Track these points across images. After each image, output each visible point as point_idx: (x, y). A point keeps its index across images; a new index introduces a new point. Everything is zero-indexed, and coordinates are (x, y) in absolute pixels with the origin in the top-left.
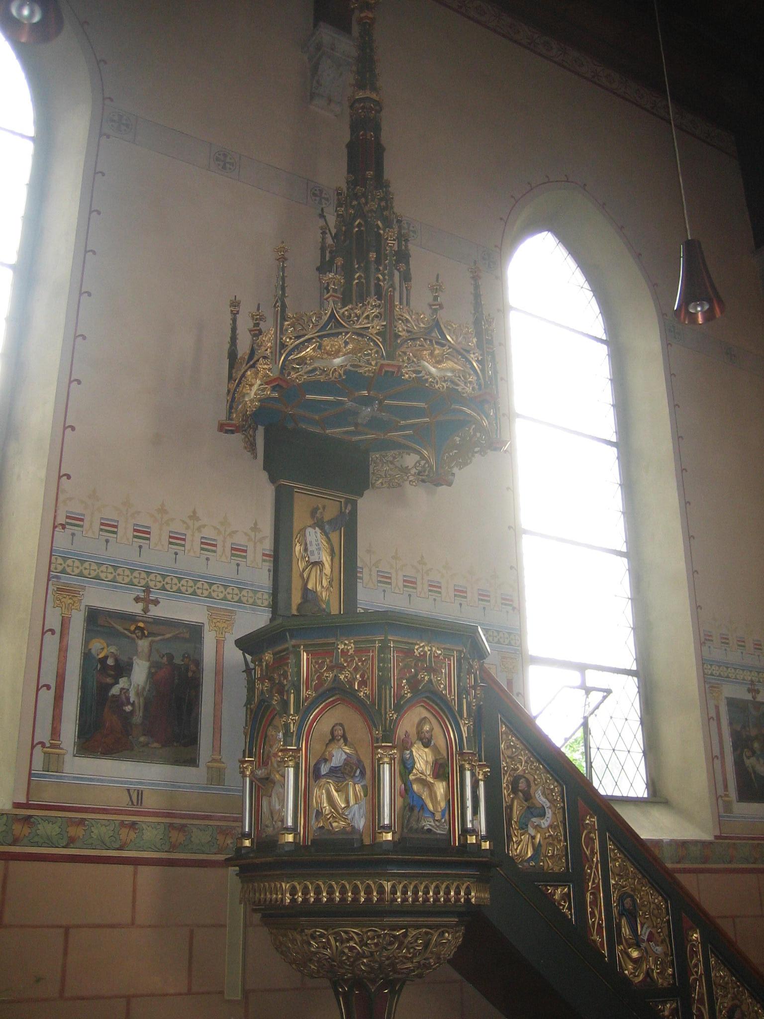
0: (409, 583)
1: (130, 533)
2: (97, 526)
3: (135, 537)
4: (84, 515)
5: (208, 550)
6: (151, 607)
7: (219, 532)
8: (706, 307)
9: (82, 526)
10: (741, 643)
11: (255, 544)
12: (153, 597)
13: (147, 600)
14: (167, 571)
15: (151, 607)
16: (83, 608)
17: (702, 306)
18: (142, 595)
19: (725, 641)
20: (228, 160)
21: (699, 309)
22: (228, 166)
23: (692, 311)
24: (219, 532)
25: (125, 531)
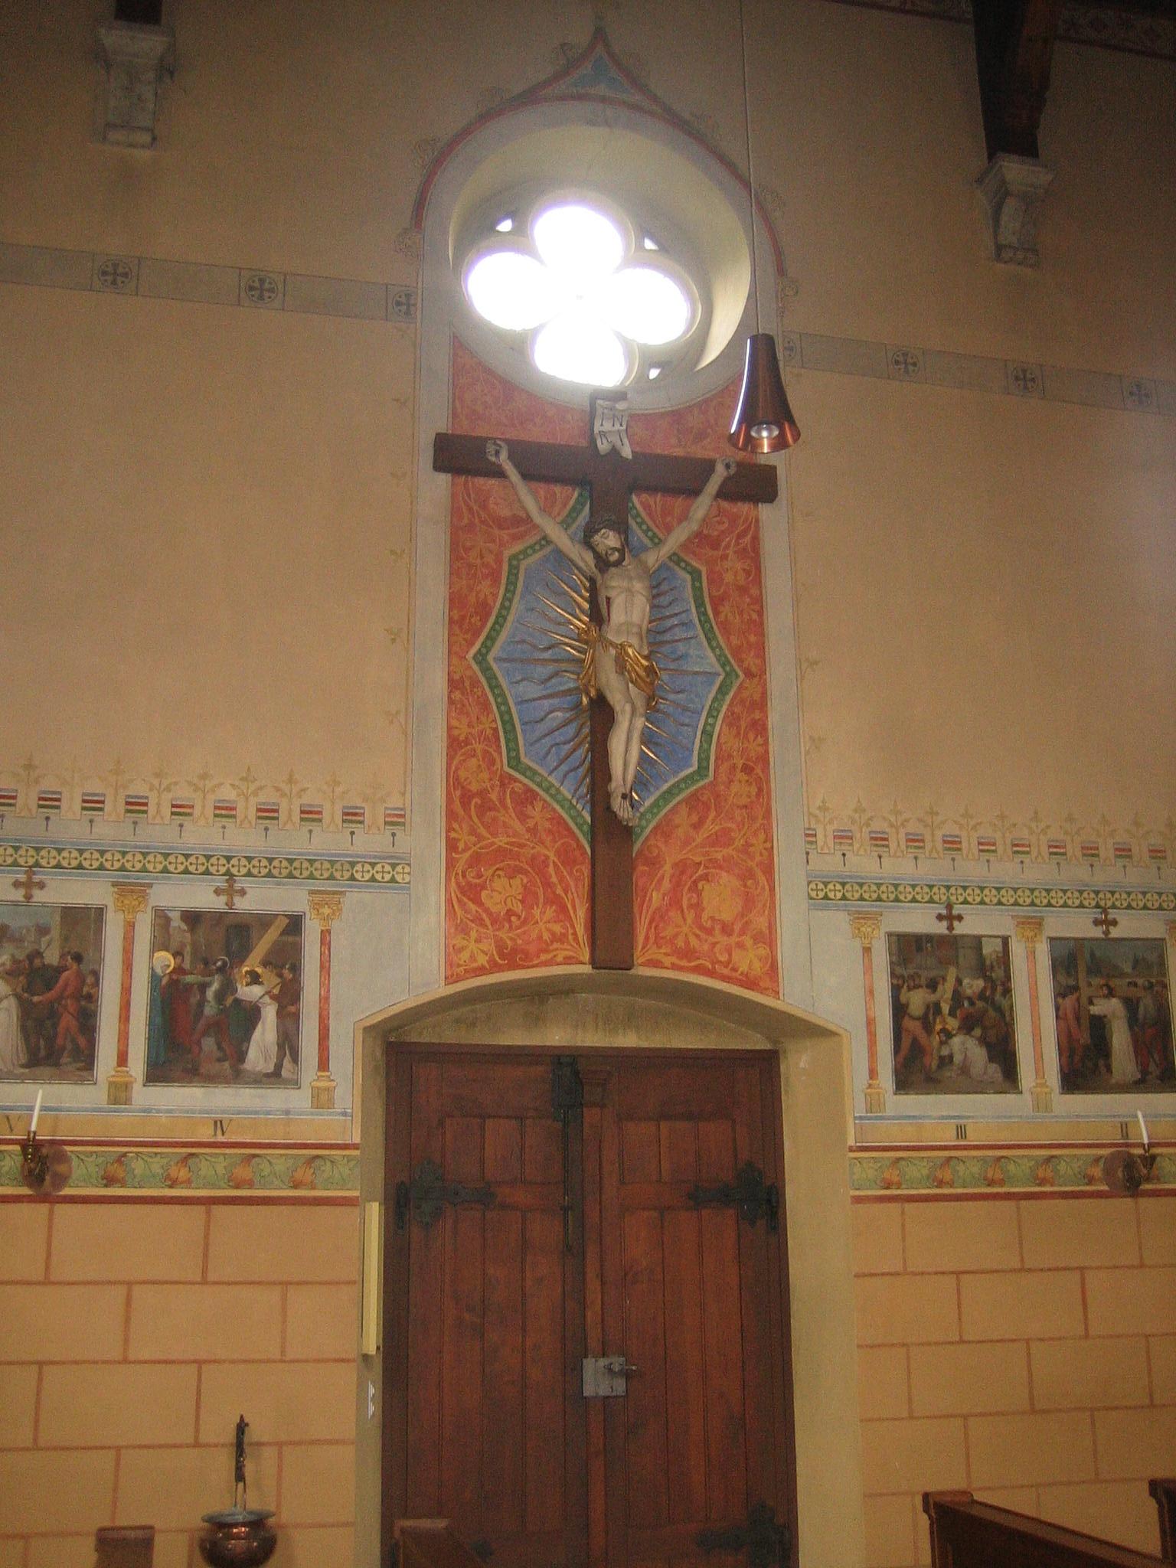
0: (136, 806)
1: (122, 807)
2: (77, 805)
3: (84, 809)
4: (60, 793)
5: (352, 822)
6: (956, 923)
7: (961, 827)
8: (776, 433)
9: (146, 812)
10: (1057, 850)
11: (116, 790)
12: (955, 912)
13: (230, 890)
14: (375, 857)
15: (956, 923)
16: (882, 935)
17: (770, 431)
18: (944, 912)
19: (843, 837)
20: (267, 286)
21: (765, 434)
22: (267, 294)
23: (753, 434)
24: (283, 795)
25: (114, 806)
